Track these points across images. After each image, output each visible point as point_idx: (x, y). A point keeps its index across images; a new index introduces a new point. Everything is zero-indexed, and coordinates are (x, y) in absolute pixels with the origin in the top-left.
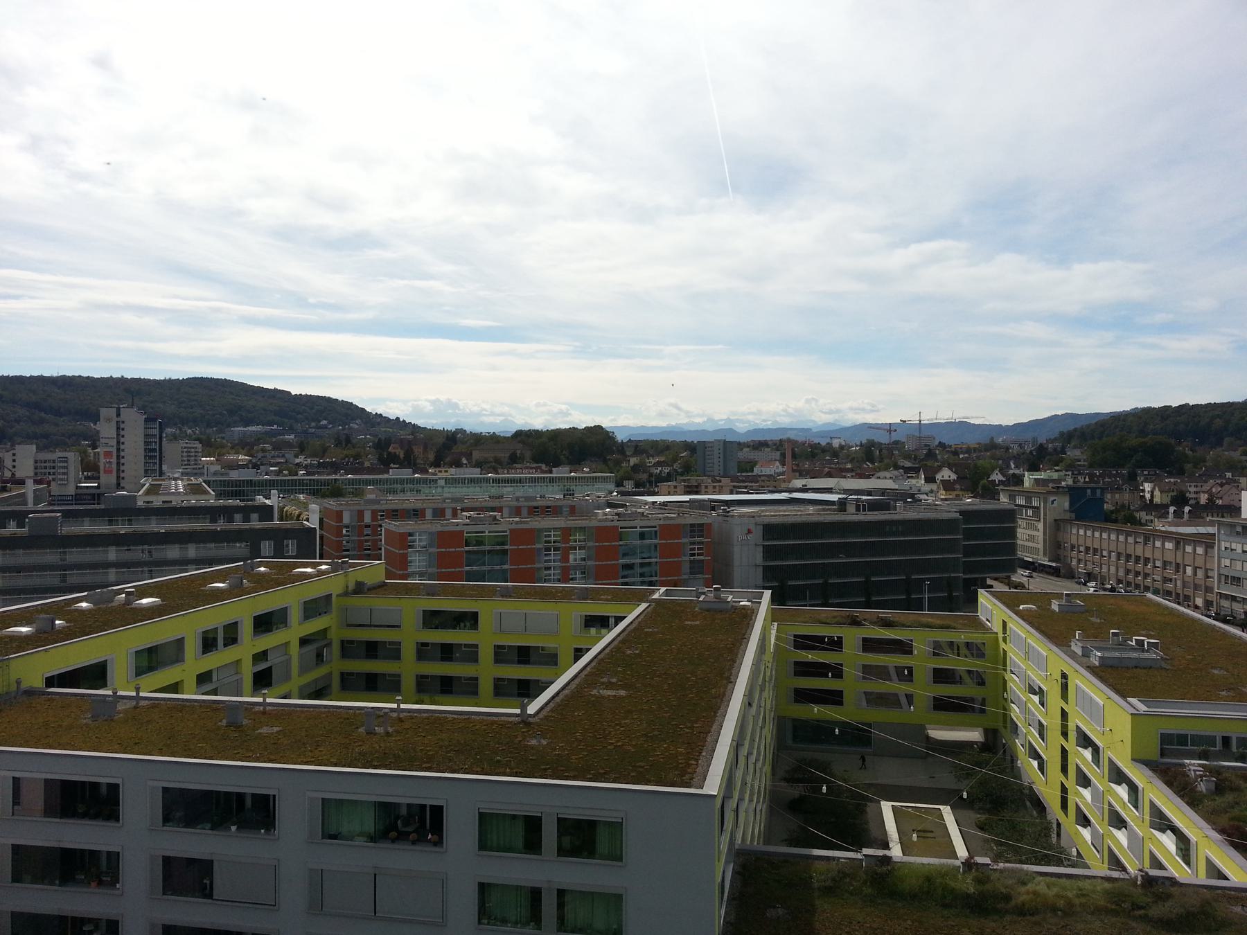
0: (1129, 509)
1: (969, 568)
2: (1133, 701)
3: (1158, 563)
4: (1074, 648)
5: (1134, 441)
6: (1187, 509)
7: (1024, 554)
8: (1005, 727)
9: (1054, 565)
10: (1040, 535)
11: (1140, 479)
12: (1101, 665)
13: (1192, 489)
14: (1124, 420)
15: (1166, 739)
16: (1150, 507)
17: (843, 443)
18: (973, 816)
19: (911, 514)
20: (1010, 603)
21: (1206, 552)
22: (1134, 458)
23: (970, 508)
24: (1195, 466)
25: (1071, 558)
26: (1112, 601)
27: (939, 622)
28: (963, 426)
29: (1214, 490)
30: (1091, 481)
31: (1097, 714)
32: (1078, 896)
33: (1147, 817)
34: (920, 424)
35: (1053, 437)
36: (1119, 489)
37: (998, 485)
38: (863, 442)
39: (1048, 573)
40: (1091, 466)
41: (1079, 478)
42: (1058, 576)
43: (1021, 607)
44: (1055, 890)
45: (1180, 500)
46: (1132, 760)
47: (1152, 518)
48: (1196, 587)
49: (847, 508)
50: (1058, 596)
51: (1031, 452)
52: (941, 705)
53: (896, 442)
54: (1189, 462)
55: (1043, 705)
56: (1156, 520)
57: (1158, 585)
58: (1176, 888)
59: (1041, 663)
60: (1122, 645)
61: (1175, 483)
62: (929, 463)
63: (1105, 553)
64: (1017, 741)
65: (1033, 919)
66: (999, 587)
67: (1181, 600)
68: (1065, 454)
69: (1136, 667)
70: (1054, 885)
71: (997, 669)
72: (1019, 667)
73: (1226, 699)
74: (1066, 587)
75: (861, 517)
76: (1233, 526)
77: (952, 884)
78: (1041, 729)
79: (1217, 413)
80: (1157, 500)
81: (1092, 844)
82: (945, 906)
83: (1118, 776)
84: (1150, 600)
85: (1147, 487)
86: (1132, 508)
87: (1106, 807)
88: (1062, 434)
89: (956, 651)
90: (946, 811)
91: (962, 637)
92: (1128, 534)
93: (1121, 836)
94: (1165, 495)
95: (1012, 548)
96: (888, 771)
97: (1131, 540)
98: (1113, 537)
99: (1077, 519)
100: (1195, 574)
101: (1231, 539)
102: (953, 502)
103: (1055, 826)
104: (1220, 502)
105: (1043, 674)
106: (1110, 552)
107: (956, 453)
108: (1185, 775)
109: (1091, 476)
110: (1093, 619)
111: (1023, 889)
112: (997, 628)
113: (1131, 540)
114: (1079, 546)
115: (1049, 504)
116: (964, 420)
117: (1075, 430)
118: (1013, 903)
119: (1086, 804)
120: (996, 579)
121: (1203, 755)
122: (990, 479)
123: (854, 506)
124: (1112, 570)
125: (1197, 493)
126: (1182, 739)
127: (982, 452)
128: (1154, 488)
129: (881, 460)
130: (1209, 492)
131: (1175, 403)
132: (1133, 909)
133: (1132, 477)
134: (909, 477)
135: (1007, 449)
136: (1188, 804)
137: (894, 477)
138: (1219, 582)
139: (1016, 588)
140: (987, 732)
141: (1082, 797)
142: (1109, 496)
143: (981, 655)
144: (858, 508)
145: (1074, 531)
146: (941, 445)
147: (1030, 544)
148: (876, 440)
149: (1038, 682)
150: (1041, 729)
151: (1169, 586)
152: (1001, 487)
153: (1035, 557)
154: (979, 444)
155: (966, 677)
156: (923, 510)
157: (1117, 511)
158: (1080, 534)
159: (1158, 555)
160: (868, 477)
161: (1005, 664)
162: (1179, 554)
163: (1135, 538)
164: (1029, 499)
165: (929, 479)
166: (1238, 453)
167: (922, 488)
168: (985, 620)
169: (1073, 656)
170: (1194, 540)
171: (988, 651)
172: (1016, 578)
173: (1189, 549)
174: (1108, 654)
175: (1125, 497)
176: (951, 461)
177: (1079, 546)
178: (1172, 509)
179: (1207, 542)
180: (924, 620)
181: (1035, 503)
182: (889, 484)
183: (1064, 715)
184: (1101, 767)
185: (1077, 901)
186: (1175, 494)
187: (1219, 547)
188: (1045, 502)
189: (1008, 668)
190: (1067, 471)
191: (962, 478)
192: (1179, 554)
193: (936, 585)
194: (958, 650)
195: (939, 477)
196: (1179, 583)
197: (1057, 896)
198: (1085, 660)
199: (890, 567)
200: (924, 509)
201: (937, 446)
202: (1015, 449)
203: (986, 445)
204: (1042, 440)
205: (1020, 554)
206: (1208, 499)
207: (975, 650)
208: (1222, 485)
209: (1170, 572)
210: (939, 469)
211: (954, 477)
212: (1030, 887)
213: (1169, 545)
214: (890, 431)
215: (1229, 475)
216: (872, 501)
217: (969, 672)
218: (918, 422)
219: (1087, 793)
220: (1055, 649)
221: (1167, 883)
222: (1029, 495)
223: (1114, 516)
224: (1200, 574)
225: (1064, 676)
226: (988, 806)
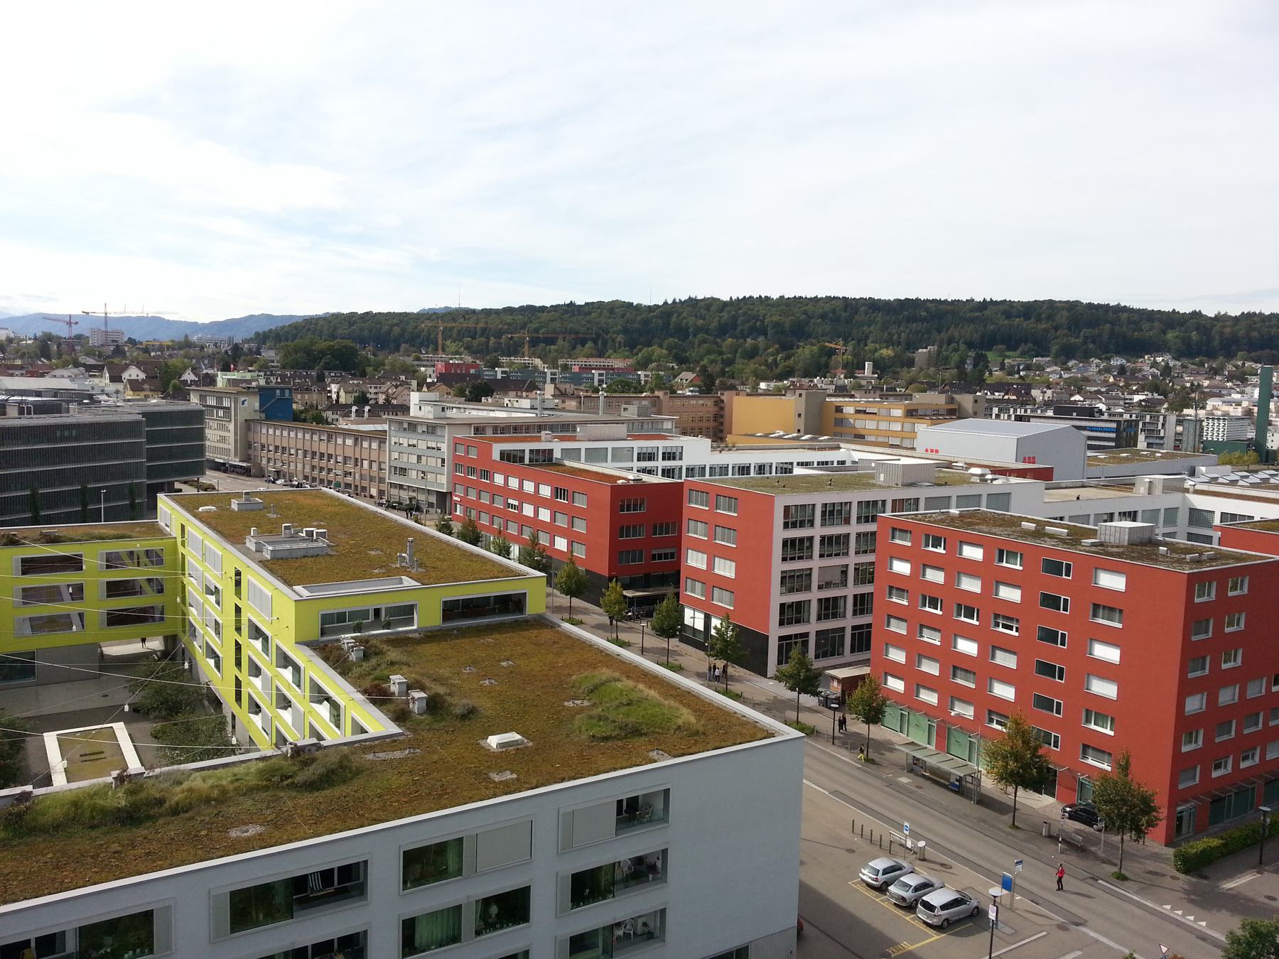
0: (317, 409)
1: (152, 472)
2: (298, 588)
3: (340, 459)
4: (248, 544)
5: (323, 345)
6: (367, 408)
7: (215, 455)
8: (184, 632)
9: (244, 465)
10: (231, 436)
11: (328, 380)
12: (272, 559)
13: (373, 390)
14: (316, 324)
15: (326, 619)
16: (336, 407)
17: (12, 335)
18: (147, 727)
19: (86, 417)
20: (190, 506)
21: (380, 447)
22: (323, 361)
23: (156, 409)
24: (375, 370)
25: (261, 457)
26: (290, 496)
27: (112, 532)
28: (157, 321)
29: (390, 391)
30: (283, 382)
31: (266, 605)
32: (232, 782)
33: (308, 694)
34: (106, 317)
35: (248, 338)
36: (308, 390)
37: (191, 385)
38: (38, 335)
39: (238, 473)
40: (283, 367)
41: (272, 378)
42: (249, 476)
43: (200, 509)
44: (210, 782)
45: (362, 400)
46: (297, 643)
47: (337, 417)
48: (372, 479)
49: (7, 410)
50: (237, 495)
51: (226, 352)
52: (116, 619)
53: (79, 337)
54: (370, 366)
55: (218, 604)
56: (341, 419)
57: (339, 479)
58: (320, 752)
59: (217, 563)
60: (294, 538)
61: (358, 385)
62: (116, 360)
63: (293, 451)
64: (195, 643)
65: (187, 815)
66: (188, 490)
67: (359, 492)
68: (260, 355)
69: (304, 557)
70: (209, 777)
71: (176, 574)
72: (197, 569)
73: (378, 576)
74: (262, 486)
75: (25, 421)
76: (401, 423)
77: (102, 802)
78: (217, 628)
79: (395, 321)
80: (342, 400)
81: (263, 728)
82: (93, 827)
83: (285, 661)
84: (325, 494)
85: (334, 388)
86: (320, 407)
87: (274, 692)
88: (257, 334)
89: (136, 561)
90: (120, 728)
91: (138, 546)
92: (313, 432)
93: (287, 715)
94: (349, 395)
95: (201, 450)
96: (57, 699)
97: (316, 438)
98: (300, 435)
99: (268, 418)
100: (371, 467)
101: (400, 434)
102: (136, 403)
103: (229, 719)
104: (395, 402)
105: (218, 573)
106: (297, 450)
107: (146, 351)
108: (340, 648)
109: (283, 377)
110: (270, 515)
111: (178, 789)
112: (176, 533)
113: (316, 438)
114: (268, 445)
115: (240, 404)
116: (157, 315)
117: (270, 331)
118: (167, 805)
119: (258, 694)
120: (185, 483)
121: (358, 628)
122: (182, 379)
123: (16, 408)
124: (299, 467)
125: (376, 393)
126: (341, 617)
127: (175, 350)
128: (340, 389)
129: (60, 356)
130: (386, 393)
131: (361, 310)
132: (282, 781)
133: (321, 378)
134: (90, 376)
135: (202, 348)
136: (340, 674)
137: (73, 376)
138: (390, 473)
139: (206, 490)
140: (166, 639)
141: (254, 687)
142: (299, 396)
143: (160, 562)
144: (21, 412)
145: (264, 431)
146: (132, 341)
147: (222, 445)
148: (54, 333)
149: (214, 582)
150: (217, 628)
151: (349, 479)
152: (193, 387)
153: (226, 458)
154: (173, 341)
155: (146, 587)
156: (101, 412)
157: (306, 411)
158: (270, 434)
159: (339, 452)
160: (42, 375)
161: (183, 569)
162: (358, 449)
163: (320, 436)
164: (220, 399)
165: (116, 379)
166: (411, 358)
167: (106, 389)
168: (164, 525)
169: (247, 553)
170: (370, 436)
171: (166, 558)
172: (207, 479)
173: (365, 444)
174: (279, 547)
175: (314, 398)
176: (140, 359)
177: (268, 445)
178: (354, 409)
179: (381, 437)
180: (96, 532)
181: (226, 403)
182: (65, 384)
183: (238, 610)
184: (270, 655)
185: (231, 787)
186: (357, 394)
187: (390, 444)
188: (236, 403)
189: (187, 572)
190: (260, 371)
191: (153, 378)
192: (358, 449)
193: (112, 494)
194: (138, 559)
195: (125, 376)
196: (357, 476)
197: (212, 787)
198: (258, 554)
199: (61, 477)
200: (103, 411)
201: (126, 342)
202: (210, 349)
203: (180, 342)
204: (238, 340)
205: (209, 455)
206: (385, 399)
207: (154, 557)
208: (396, 387)
209: (350, 467)
210: (126, 367)
211: (142, 376)
212: (185, 785)
213: (349, 442)
214: (70, 323)
215: (403, 378)
216: (39, 403)
217: (149, 580)
218: (104, 315)
219: (257, 682)
220: (230, 547)
221: (313, 749)
222: (220, 395)
223: (303, 416)
224: (375, 466)
225: (238, 573)
226: (164, 713)
